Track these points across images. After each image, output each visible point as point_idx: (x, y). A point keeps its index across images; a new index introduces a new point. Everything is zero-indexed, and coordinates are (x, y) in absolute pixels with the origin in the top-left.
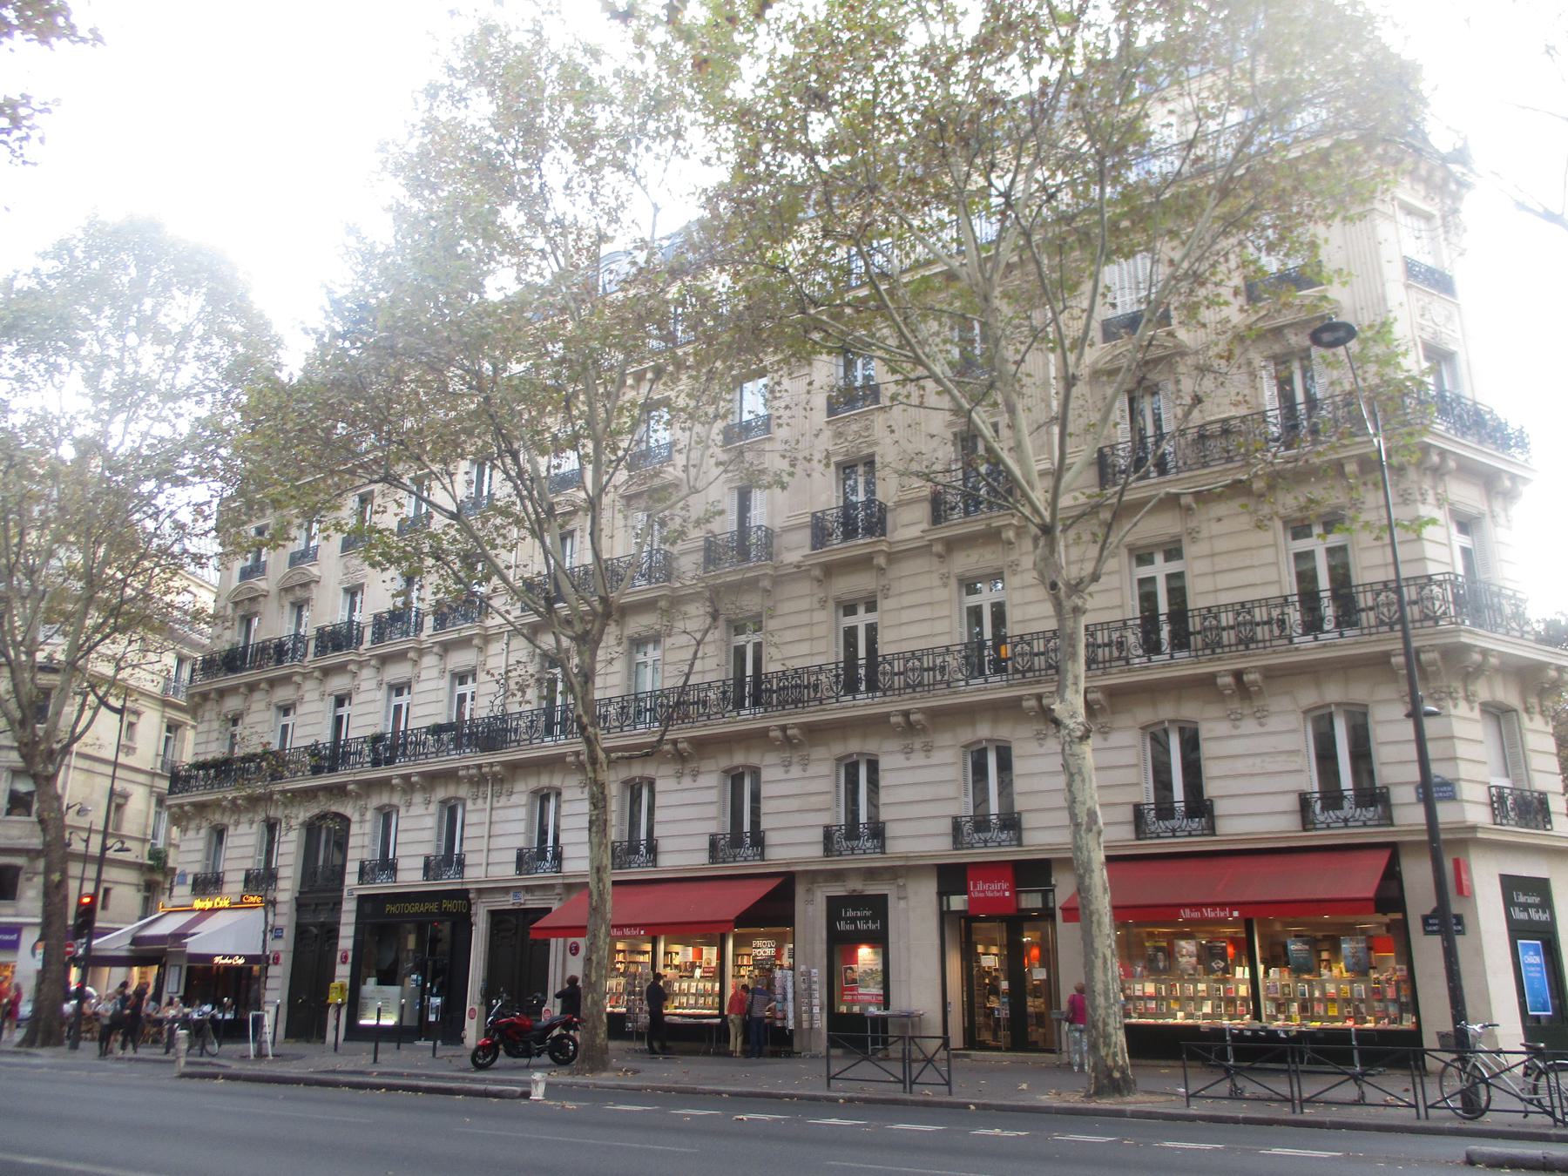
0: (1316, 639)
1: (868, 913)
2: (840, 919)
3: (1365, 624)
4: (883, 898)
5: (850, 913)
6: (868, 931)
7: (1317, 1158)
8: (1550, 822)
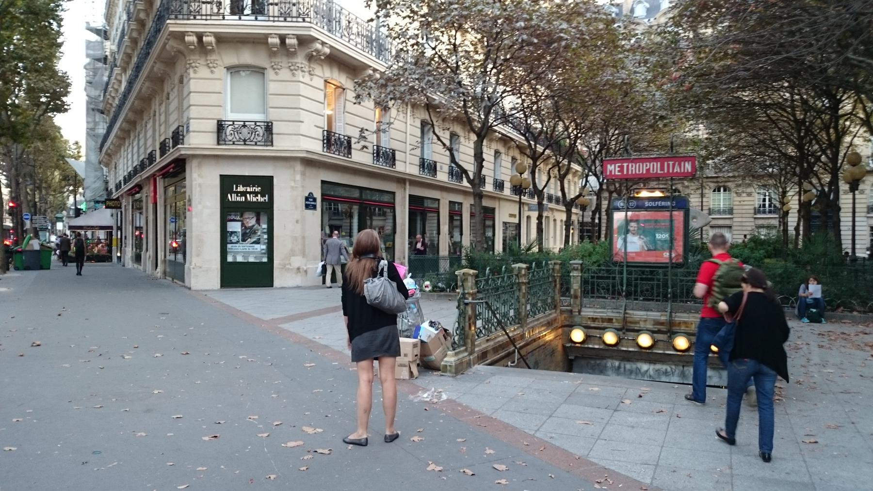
0: (240, 19)
1: (258, 189)
3: (271, 14)
5: (241, 189)
6: (257, 203)
8: (350, 154)
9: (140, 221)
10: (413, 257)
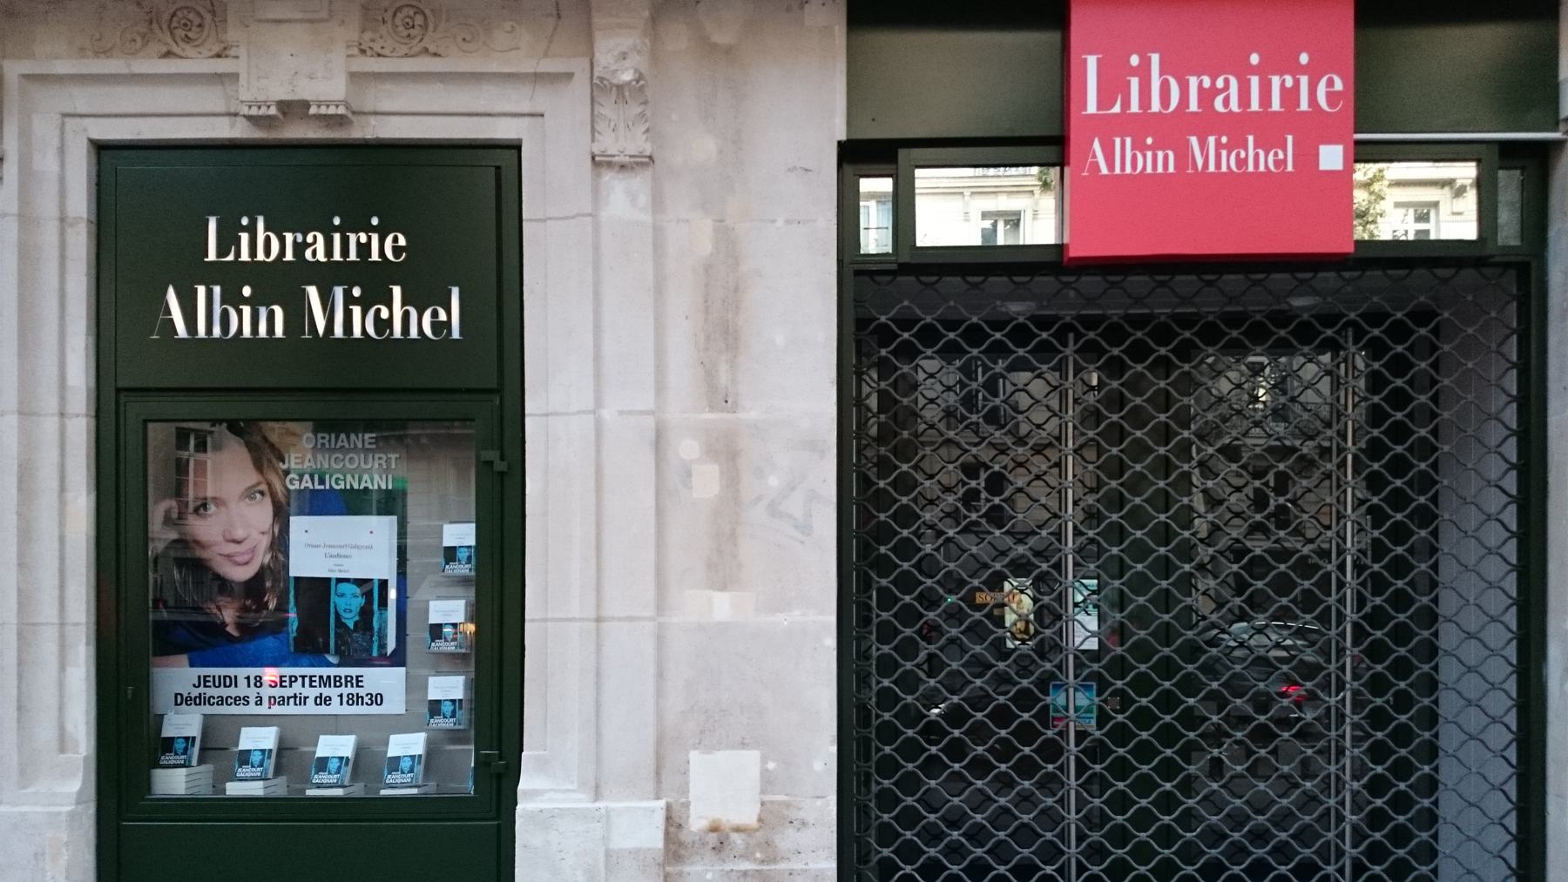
1: (386, 247)
2: (190, 272)
4: (492, 170)
5: (262, 244)
6: (382, 347)
7: (1527, 130)
9: (310, 701)
10: (332, 659)
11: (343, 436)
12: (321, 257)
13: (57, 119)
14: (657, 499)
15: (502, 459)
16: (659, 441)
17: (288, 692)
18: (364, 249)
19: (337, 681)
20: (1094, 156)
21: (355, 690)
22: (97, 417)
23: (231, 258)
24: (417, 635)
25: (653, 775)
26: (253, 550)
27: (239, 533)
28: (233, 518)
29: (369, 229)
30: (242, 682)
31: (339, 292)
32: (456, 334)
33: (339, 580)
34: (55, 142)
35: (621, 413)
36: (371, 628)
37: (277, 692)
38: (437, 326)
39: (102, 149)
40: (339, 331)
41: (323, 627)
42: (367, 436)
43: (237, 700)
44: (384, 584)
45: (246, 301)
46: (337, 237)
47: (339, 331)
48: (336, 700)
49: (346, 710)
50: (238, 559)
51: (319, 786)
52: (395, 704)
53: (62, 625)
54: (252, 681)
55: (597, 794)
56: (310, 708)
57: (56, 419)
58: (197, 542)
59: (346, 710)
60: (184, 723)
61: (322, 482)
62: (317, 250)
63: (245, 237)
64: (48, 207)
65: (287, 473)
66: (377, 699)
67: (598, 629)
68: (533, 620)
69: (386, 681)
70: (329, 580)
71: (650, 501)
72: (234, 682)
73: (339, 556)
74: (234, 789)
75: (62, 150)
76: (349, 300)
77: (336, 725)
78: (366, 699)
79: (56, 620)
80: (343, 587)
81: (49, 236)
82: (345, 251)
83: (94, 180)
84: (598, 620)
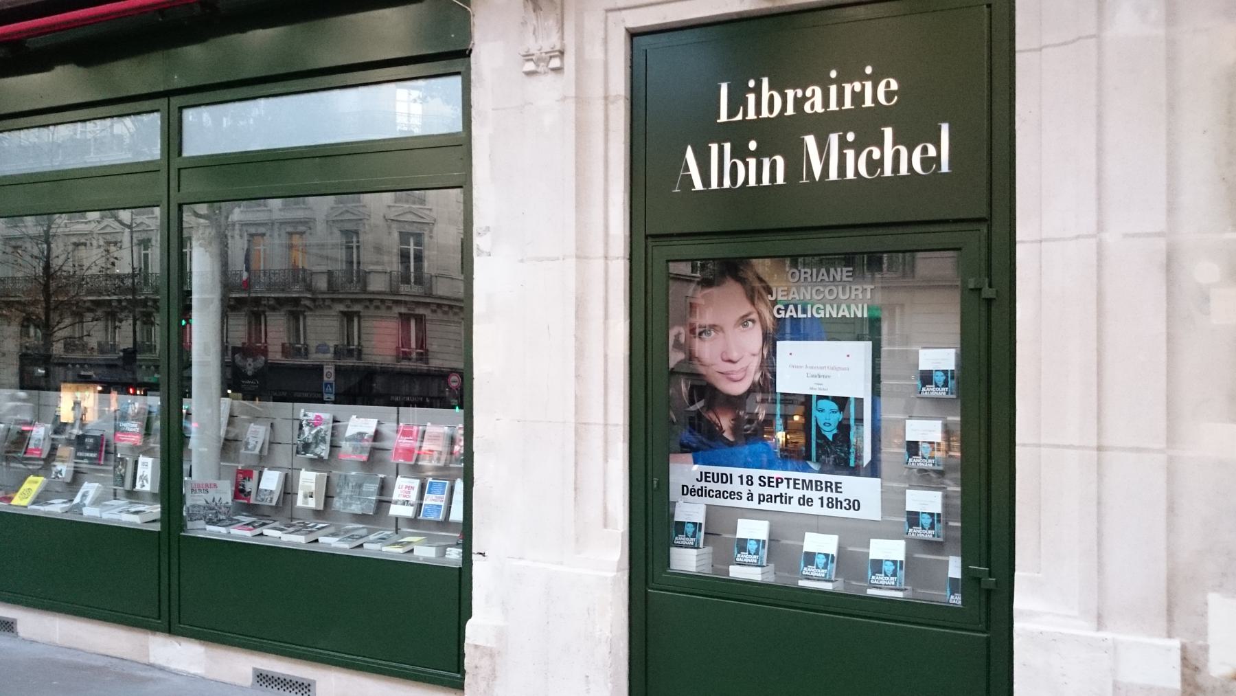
1: (878, 92)
6: (876, 185)
9: (795, 501)
11: (823, 270)
12: (819, 109)
13: (602, 14)
14: (1169, 326)
15: (990, 286)
16: (1171, 264)
17: (774, 491)
18: (858, 97)
19: (818, 485)
20: (687, 169)
21: (834, 495)
22: (631, 259)
23: (739, 117)
24: (892, 451)
25: (1165, 612)
26: (746, 369)
27: (735, 356)
28: (729, 345)
29: (863, 77)
30: (736, 480)
31: (834, 139)
32: (945, 168)
33: (820, 397)
34: (601, 34)
35: (1126, 235)
36: (848, 440)
37: (766, 491)
38: (926, 162)
39: (634, 35)
40: (833, 175)
41: (826, 442)
42: (845, 269)
43: (732, 494)
44: (859, 401)
45: (752, 154)
46: (833, 89)
47: (833, 175)
48: (817, 502)
49: (826, 511)
50: (734, 377)
51: (808, 578)
52: (871, 510)
53: (606, 425)
54: (745, 480)
55: (1100, 623)
56: (794, 507)
57: (602, 261)
58: (699, 360)
59: (826, 511)
60: (690, 511)
61: (804, 311)
62: (815, 104)
63: (751, 98)
64: (596, 91)
65: (775, 303)
66: (854, 505)
67: (1099, 463)
68: (1024, 445)
69: (863, 490)
70: (810, 396)
71: (1161, 327)
72: (729, 479)
73: (819, 376)
74: (736, 572)
75: (605, 41)
76: (843, 144)
77: (820, 525)
78: (845, 504)
79: (602, 421)
80: (822, 403)
81: (596, 112)
82: (840, 101)
83: (629, 63)
84: (1100, 448)
